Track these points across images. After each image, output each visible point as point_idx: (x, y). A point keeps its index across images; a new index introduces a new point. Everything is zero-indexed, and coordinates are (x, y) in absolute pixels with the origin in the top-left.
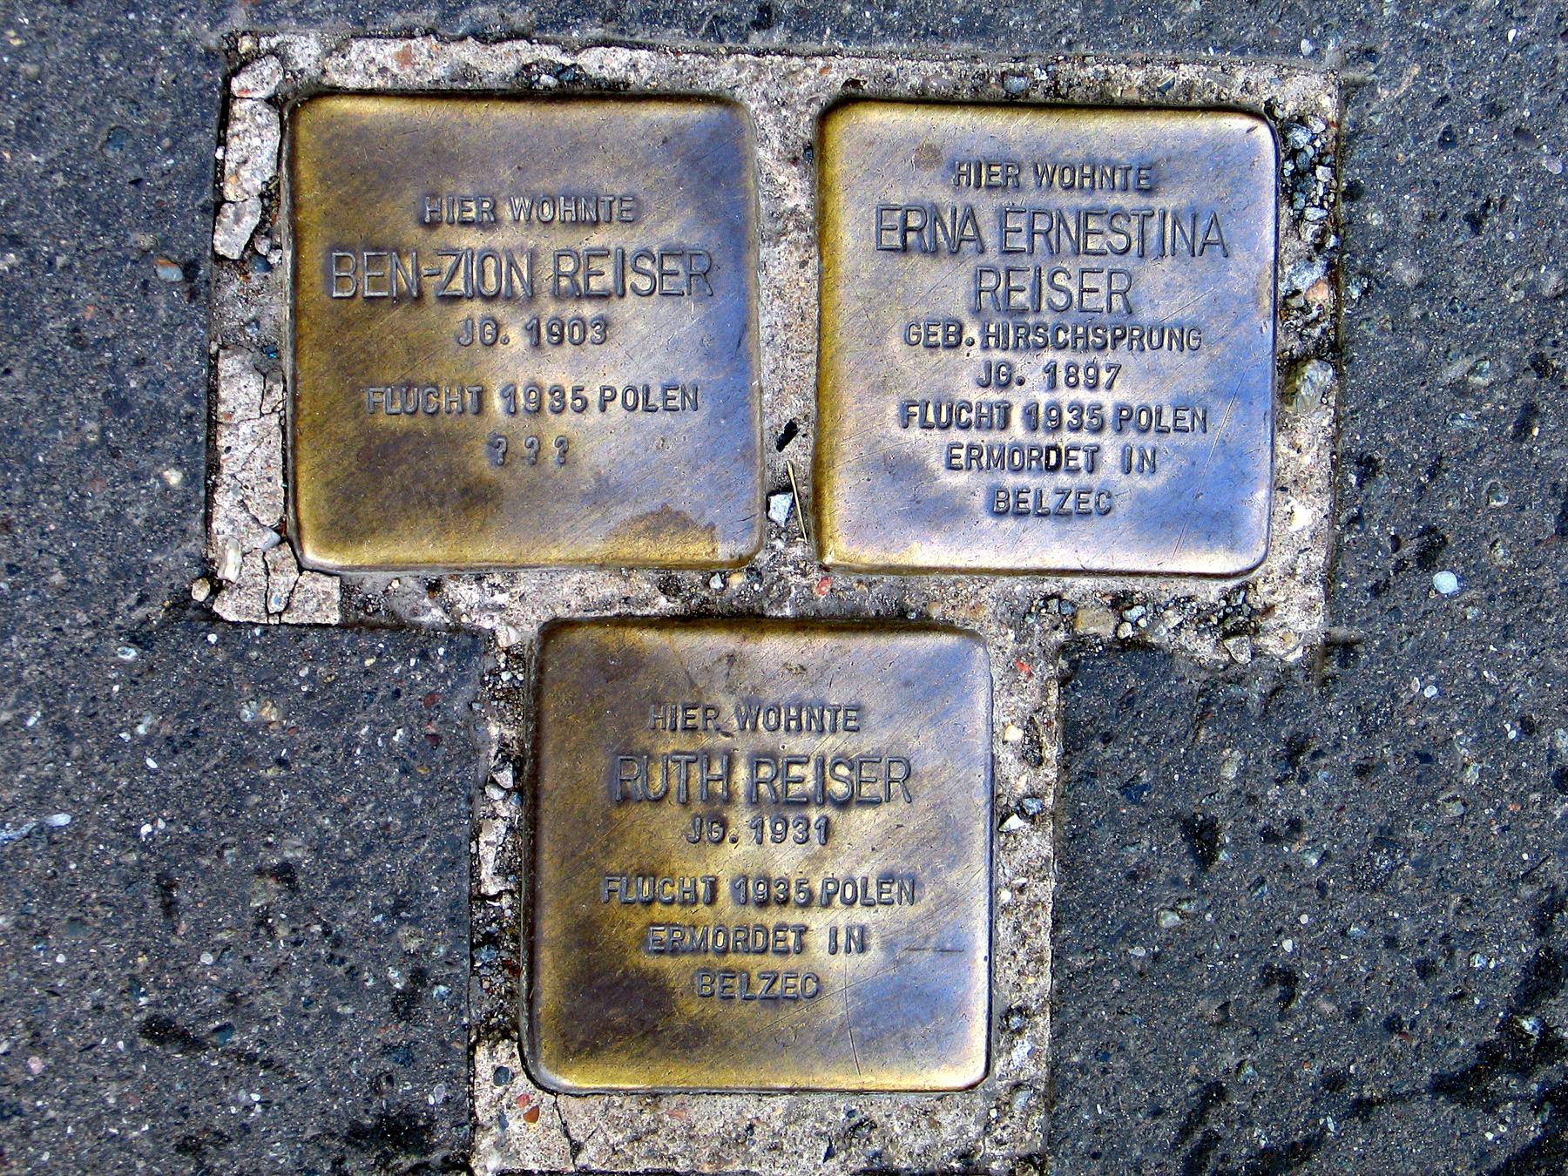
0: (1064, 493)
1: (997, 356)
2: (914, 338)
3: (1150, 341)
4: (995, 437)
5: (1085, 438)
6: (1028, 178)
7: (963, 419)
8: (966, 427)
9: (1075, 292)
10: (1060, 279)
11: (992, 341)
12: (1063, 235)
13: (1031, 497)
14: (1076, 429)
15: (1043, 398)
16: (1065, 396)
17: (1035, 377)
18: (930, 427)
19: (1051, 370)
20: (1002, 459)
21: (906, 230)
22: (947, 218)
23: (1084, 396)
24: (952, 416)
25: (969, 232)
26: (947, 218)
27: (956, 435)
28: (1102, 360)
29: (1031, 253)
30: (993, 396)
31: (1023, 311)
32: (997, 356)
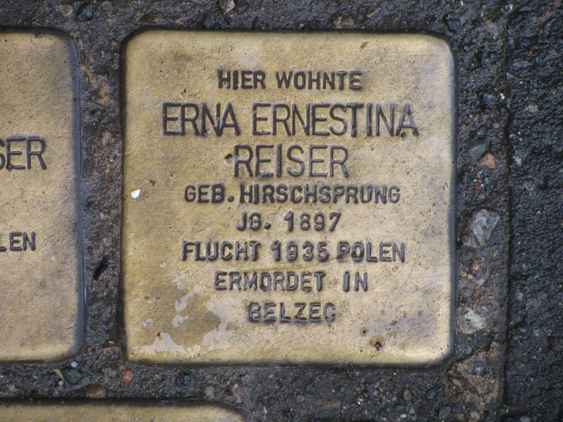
0: (301, 305)
1: (251, 209)
2: (191, 197)
3: (362, 196)
4: (248, 266)
5: (316, 266)
6: (271, 82)
7: (226, 254)
8: (228, 259)
9: (307, 164)
10: (296, 154)
11: (247, 198)
12: (382, 122)
13: (277, 309)
14: (309, 259)
15: (285, 241)
16: (300, 237)
17: (280, 225)
18: (203, 259)
19: (290, 219)
20: (259, 282)
21: (184, 120)
22: (214, 113)
23: (315, 238)
24: (219, 251)
25: (230, 121)
26: (214, 113)
27: (221, 266)
28: (327, 210)
29: (275, 133)
30: (246, 237)
31: (268, 176)
32: (251, 209)
